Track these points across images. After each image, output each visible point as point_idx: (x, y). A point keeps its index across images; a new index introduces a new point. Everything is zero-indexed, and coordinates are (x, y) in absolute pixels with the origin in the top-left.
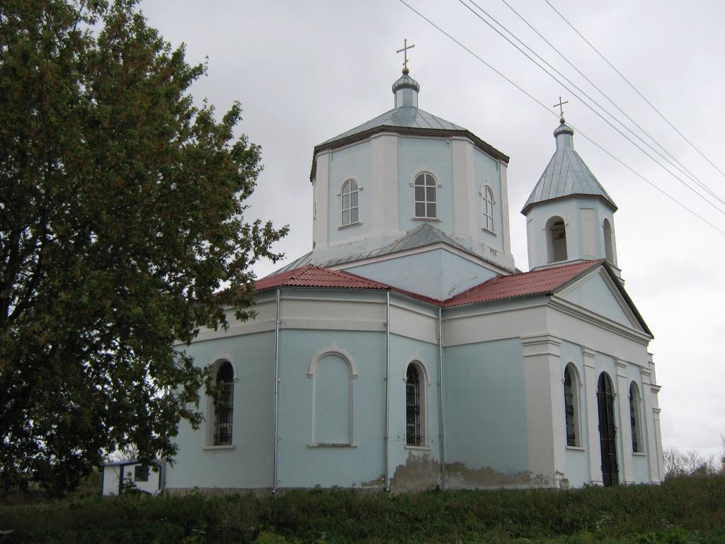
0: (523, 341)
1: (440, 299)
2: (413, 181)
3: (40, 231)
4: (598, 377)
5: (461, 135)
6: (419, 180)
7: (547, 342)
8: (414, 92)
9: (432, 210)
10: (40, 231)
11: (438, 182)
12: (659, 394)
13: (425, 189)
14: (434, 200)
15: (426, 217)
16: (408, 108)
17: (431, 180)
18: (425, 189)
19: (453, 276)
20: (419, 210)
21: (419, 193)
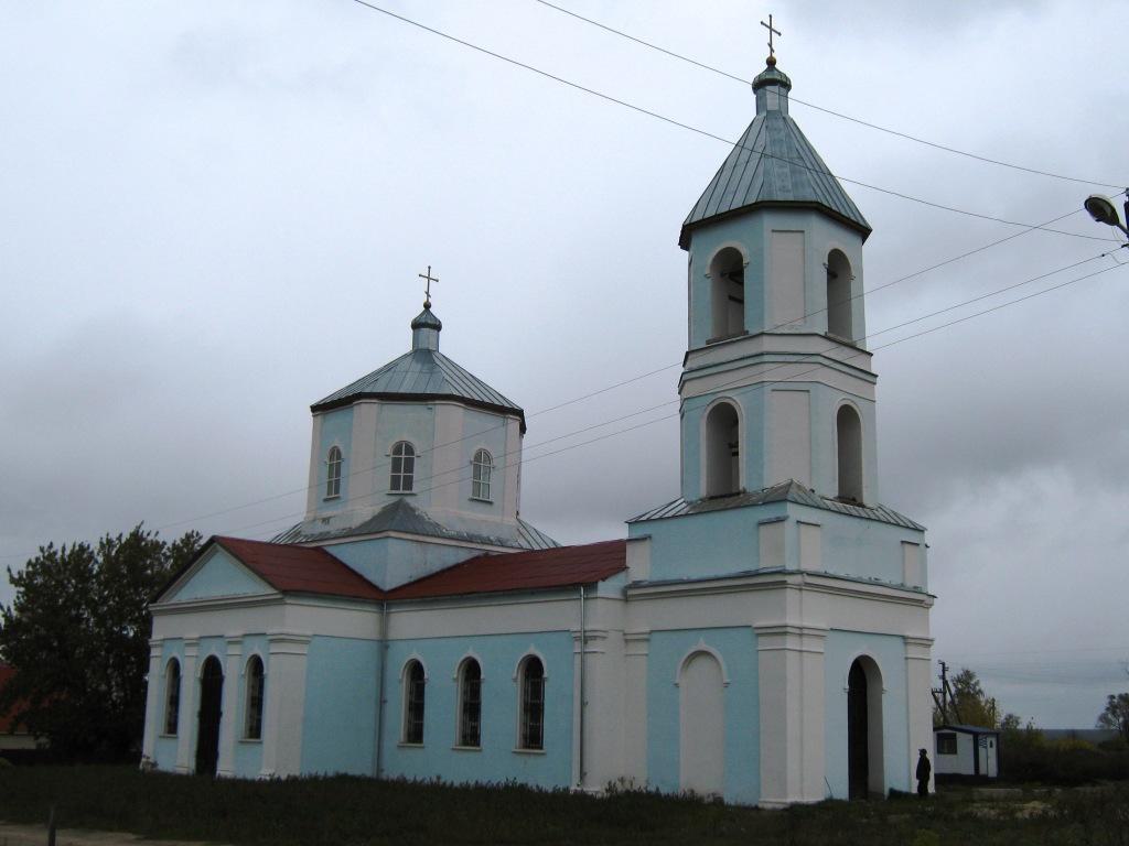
0: (573, 635)
1: (381, 587)
2: (389, 451)
3: (1115, 700)
4: (196, 714)
5: (459, 402)
6: (397, 450)
7: (785, 633)
8: (434, 332)
9: (409, 483)
10: (1115, 700)
11: (417, 452)
12: (931, 610)
13: (403, 461)
14: (412, 471)
15: (401, 491)
16: (424, 354)
17: (410, 450)
18: (403, 461)
19: (394, 562)
20: (395, 483)
21: (396, 466)
